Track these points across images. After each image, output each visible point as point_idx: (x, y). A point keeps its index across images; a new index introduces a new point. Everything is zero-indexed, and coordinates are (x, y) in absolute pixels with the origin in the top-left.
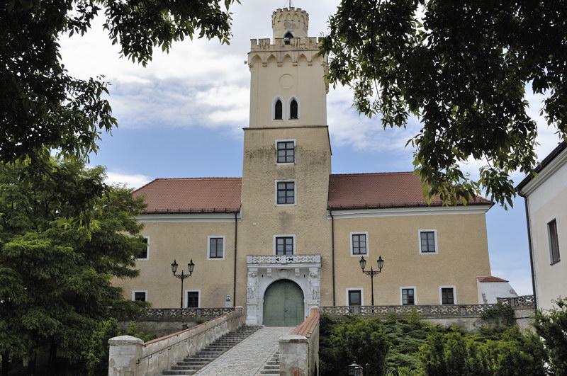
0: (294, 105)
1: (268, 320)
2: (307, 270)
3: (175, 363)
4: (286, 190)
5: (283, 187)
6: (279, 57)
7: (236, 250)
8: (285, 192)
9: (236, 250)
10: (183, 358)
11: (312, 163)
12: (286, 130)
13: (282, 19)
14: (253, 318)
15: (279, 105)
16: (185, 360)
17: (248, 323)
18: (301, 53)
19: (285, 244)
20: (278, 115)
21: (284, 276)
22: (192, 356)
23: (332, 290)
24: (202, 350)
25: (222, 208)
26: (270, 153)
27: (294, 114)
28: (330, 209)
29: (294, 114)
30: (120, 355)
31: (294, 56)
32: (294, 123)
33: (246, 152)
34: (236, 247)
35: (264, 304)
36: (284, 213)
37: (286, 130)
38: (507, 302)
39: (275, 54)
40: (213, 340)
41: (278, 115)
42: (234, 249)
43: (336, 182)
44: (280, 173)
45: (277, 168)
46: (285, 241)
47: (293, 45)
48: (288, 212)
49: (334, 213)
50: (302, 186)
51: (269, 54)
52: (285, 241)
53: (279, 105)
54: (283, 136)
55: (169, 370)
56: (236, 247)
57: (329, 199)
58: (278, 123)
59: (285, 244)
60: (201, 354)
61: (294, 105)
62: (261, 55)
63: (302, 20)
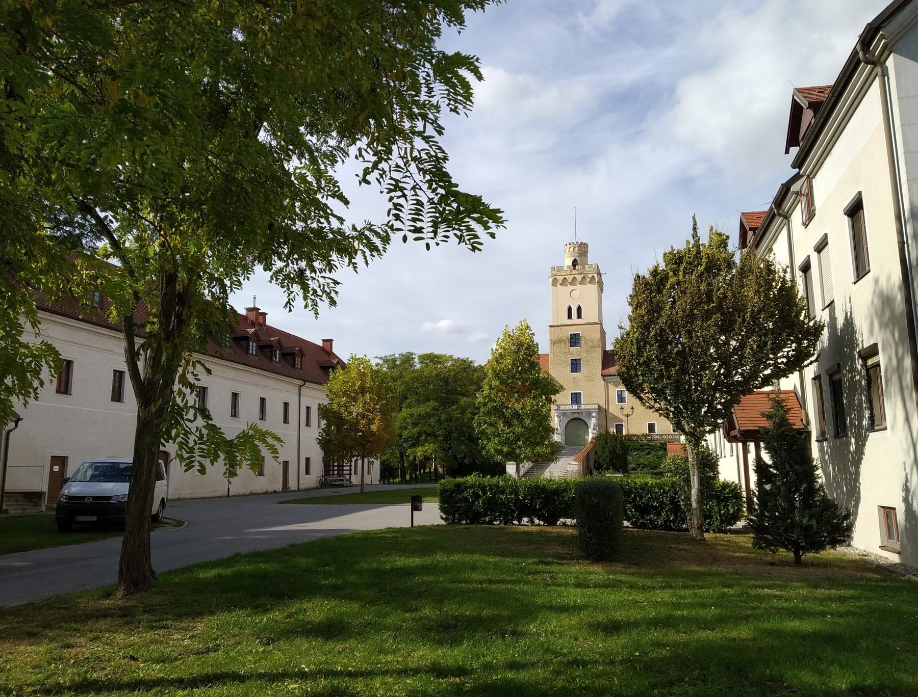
0: (579, 309)
8: (575, 366)
12: (297, 433)
15: (570, 309)
20: (570, 317)
21: (576, 416)
27: (579, 316)
28: (603, 376)
29: (579, 316)
31: (579, 277)
32: (579, 321)
37: (575, 326)
40: (515, 560)
41: (570, 317)
50: (369, 63)
53: (570, 309)
54: (573, 330)
57: (603, 369)
58: (570, 322)
61: (579, 309)
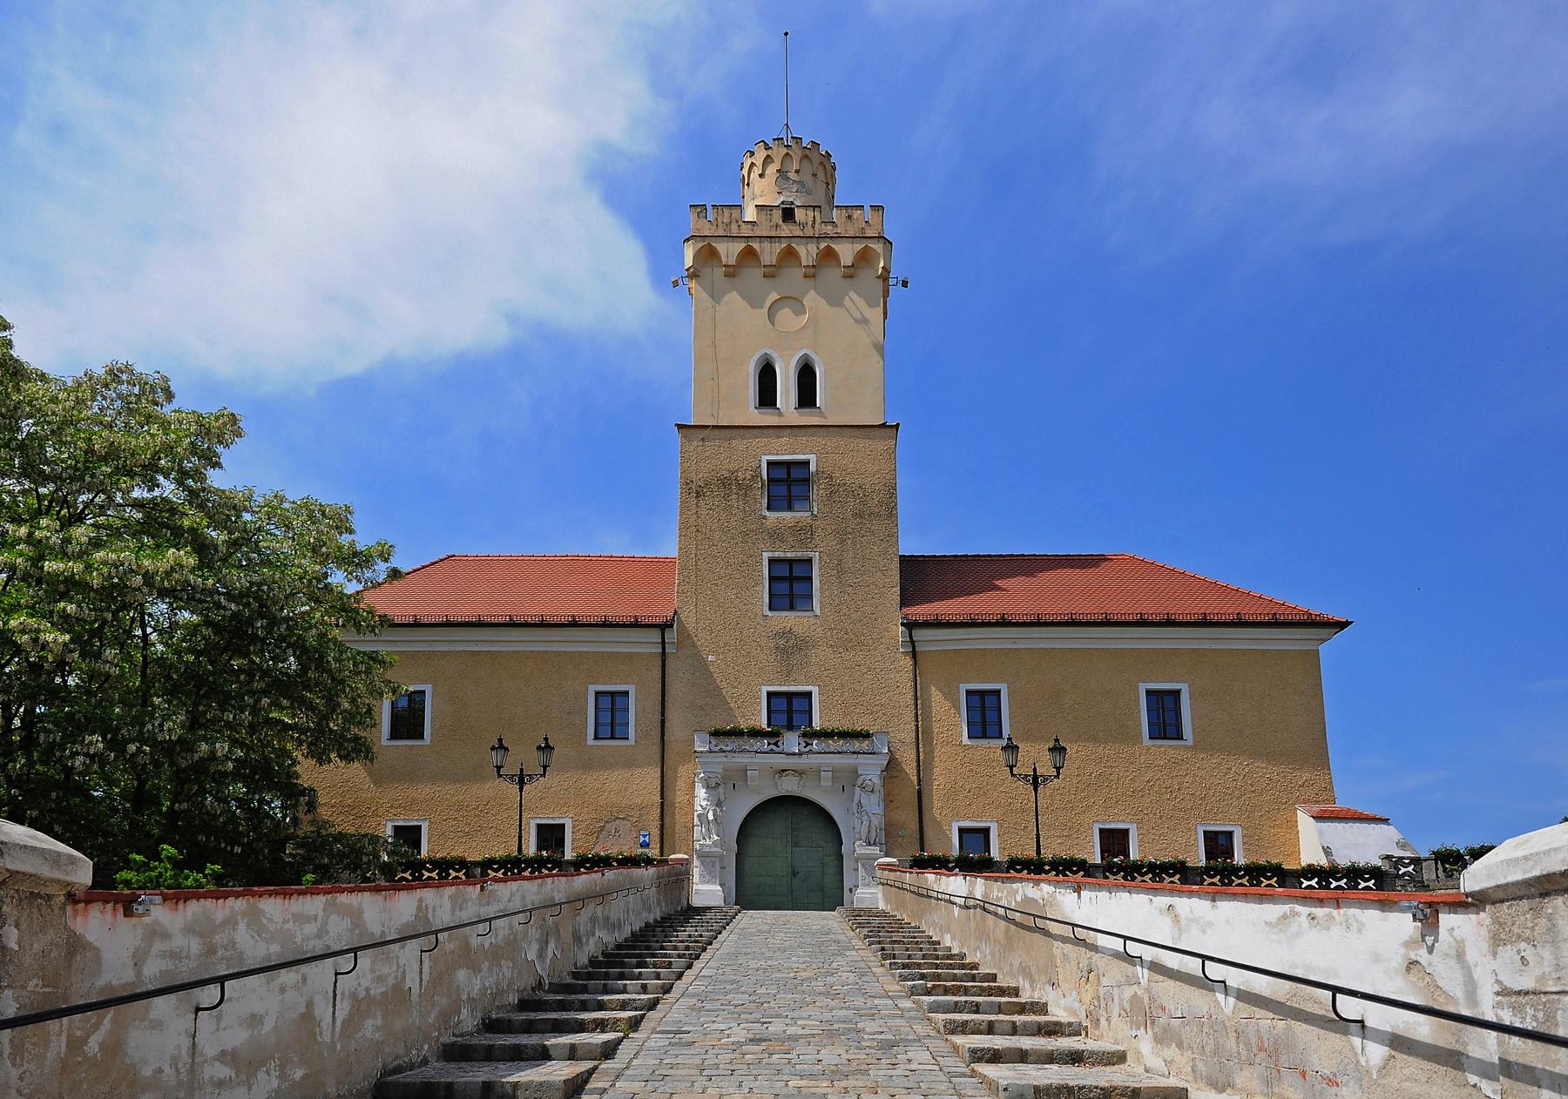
0: (806, 375)
1: (747, 896)
2: (854, 773)
3: (468, 1020)
4: (791, 579)
5: (783, 571)
6: (769, 253)
7: (663, 722)
8: (790, 583)
9: (663, 722)
10: (513, 999)
11: (859, 515)
13: (772, 169)
14: (706, 890)
15: (767, 375)
16: (524, 1005)
17: (696, 902)
18: (823, 245)
19: (790, 712)
20: (767, 396)
21: (789, 786)
22: (556, 988)
23: (915, 826)
24: (593, 962)
25: (624, 612)
26: (749, 488)
27: (807, 396)
29: (807, 396)
30: (794, 874)
33: (687, 483)
34: (663, 714)
35: (737, 855)
36: (787, 634)
38: (1410, 869)
39: (756, 245)
41: (767, 396)
42: (658, 716)
43: (921, 577)
44: (775, 536)
45: (768, 524)
46: (790, 704)
47: (804, 225)
48: (798, 630)
49: (919, 634)
51: (741, 246)
52: (790, 704)
53: (767, 375)
55: (569, 980)
56: (663, 714)
57: (905, 601)
59: (790, 712)
60: (590, 976)
61: (806, 375)
62: (721, 247)
63: (821, 175)
